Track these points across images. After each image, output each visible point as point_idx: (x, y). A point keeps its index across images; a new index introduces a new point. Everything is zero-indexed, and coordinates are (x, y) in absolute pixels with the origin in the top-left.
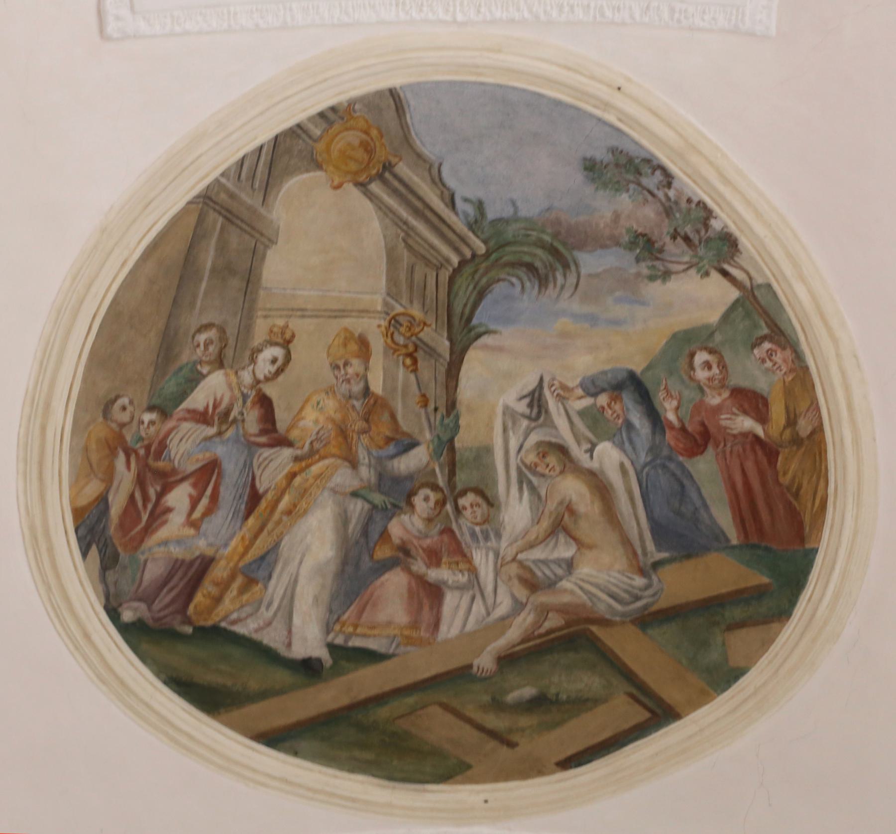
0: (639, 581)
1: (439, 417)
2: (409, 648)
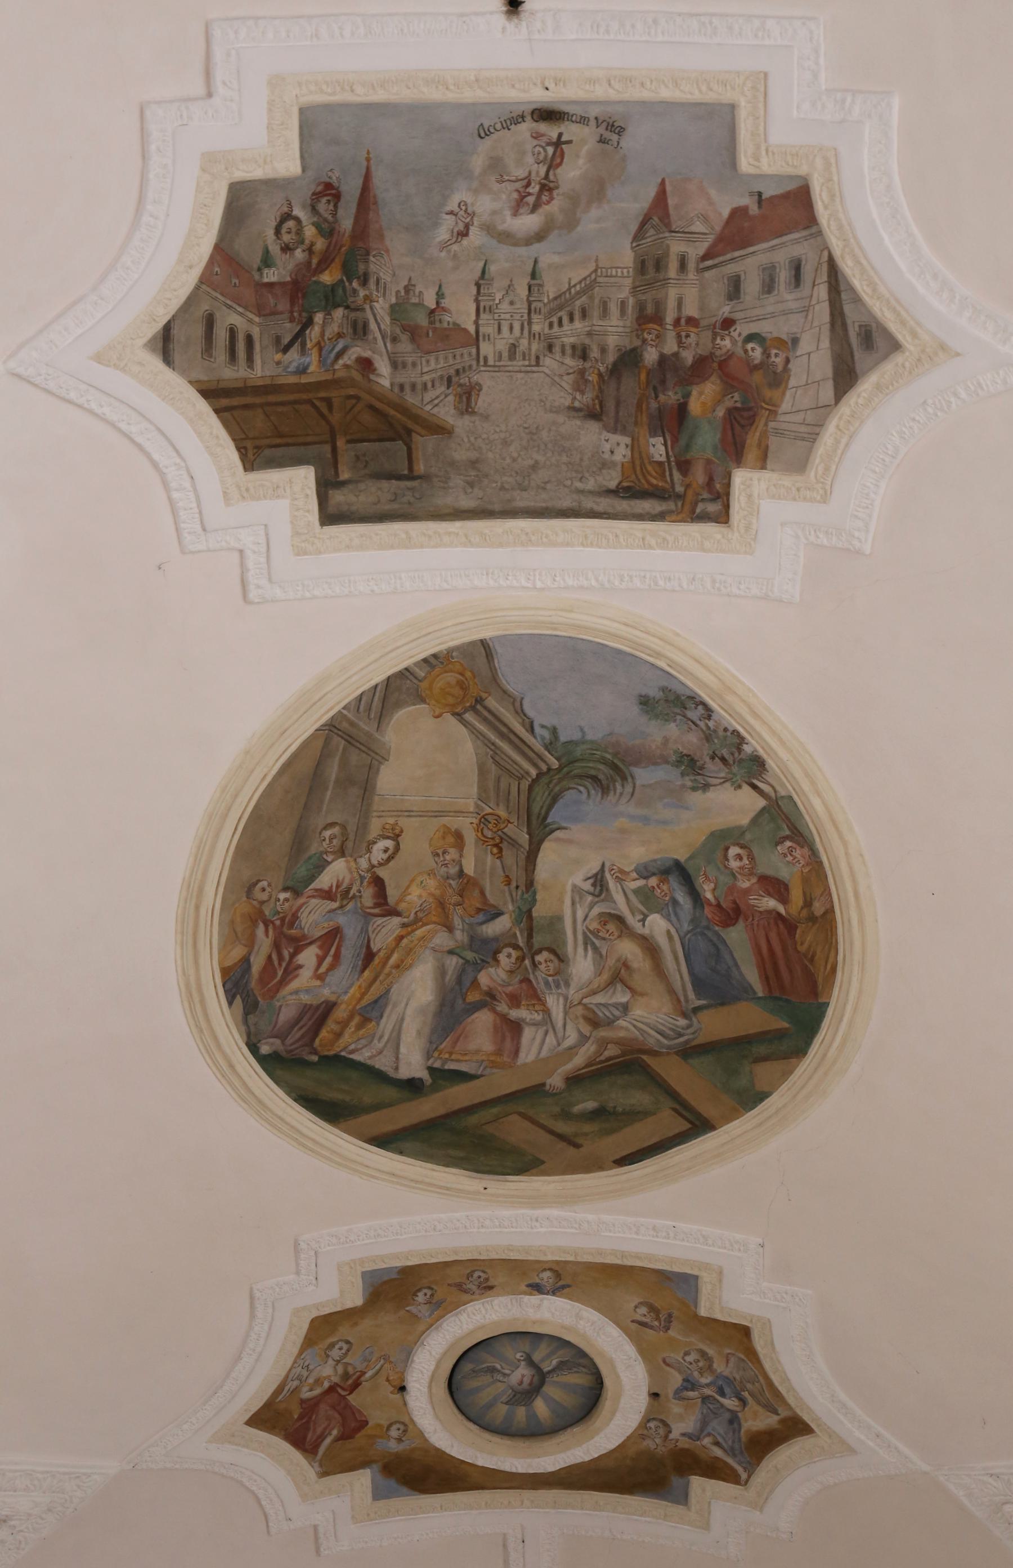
0: (682, 1022)
1: (520, 892)
2: (495, 1070)
